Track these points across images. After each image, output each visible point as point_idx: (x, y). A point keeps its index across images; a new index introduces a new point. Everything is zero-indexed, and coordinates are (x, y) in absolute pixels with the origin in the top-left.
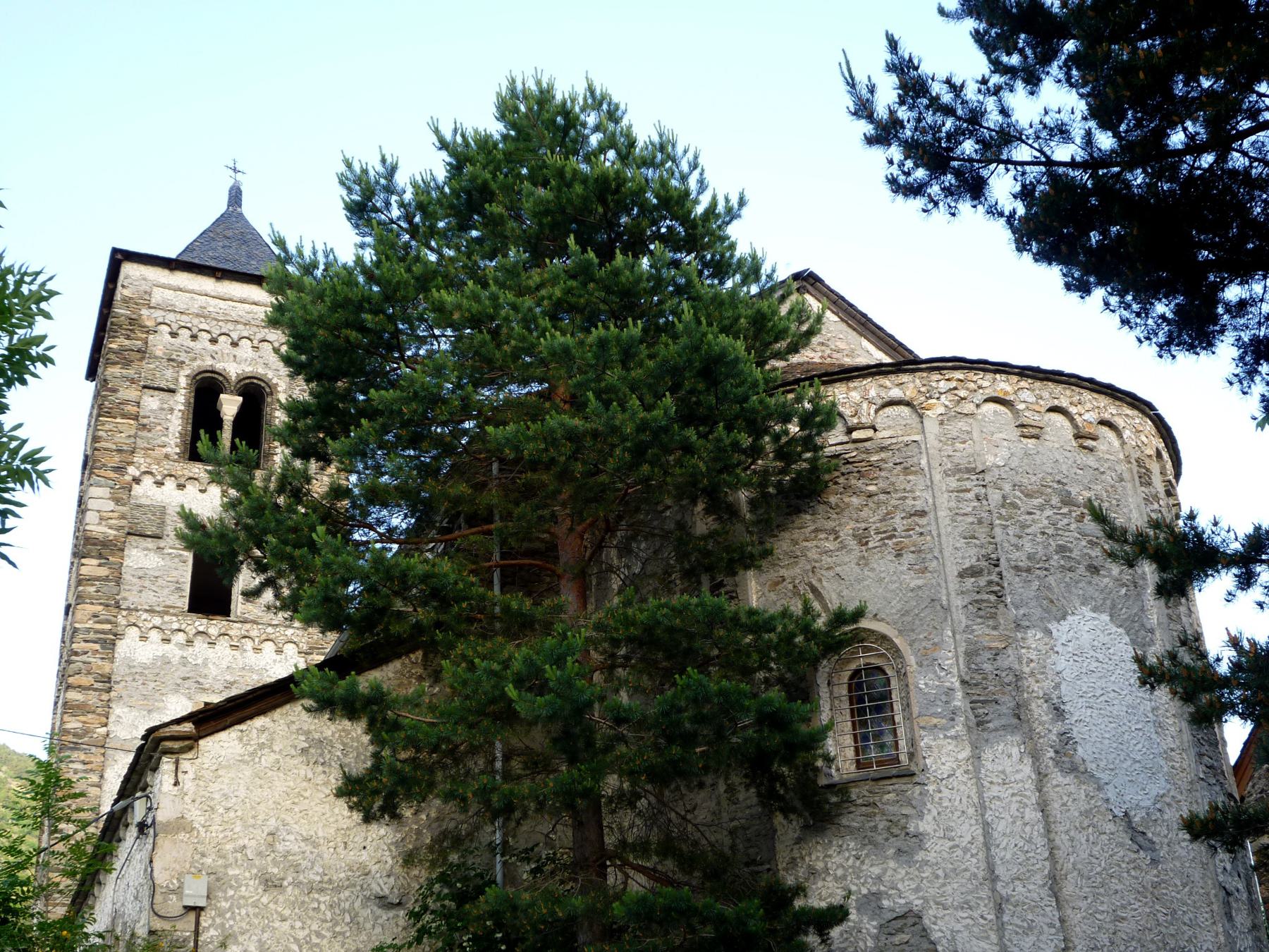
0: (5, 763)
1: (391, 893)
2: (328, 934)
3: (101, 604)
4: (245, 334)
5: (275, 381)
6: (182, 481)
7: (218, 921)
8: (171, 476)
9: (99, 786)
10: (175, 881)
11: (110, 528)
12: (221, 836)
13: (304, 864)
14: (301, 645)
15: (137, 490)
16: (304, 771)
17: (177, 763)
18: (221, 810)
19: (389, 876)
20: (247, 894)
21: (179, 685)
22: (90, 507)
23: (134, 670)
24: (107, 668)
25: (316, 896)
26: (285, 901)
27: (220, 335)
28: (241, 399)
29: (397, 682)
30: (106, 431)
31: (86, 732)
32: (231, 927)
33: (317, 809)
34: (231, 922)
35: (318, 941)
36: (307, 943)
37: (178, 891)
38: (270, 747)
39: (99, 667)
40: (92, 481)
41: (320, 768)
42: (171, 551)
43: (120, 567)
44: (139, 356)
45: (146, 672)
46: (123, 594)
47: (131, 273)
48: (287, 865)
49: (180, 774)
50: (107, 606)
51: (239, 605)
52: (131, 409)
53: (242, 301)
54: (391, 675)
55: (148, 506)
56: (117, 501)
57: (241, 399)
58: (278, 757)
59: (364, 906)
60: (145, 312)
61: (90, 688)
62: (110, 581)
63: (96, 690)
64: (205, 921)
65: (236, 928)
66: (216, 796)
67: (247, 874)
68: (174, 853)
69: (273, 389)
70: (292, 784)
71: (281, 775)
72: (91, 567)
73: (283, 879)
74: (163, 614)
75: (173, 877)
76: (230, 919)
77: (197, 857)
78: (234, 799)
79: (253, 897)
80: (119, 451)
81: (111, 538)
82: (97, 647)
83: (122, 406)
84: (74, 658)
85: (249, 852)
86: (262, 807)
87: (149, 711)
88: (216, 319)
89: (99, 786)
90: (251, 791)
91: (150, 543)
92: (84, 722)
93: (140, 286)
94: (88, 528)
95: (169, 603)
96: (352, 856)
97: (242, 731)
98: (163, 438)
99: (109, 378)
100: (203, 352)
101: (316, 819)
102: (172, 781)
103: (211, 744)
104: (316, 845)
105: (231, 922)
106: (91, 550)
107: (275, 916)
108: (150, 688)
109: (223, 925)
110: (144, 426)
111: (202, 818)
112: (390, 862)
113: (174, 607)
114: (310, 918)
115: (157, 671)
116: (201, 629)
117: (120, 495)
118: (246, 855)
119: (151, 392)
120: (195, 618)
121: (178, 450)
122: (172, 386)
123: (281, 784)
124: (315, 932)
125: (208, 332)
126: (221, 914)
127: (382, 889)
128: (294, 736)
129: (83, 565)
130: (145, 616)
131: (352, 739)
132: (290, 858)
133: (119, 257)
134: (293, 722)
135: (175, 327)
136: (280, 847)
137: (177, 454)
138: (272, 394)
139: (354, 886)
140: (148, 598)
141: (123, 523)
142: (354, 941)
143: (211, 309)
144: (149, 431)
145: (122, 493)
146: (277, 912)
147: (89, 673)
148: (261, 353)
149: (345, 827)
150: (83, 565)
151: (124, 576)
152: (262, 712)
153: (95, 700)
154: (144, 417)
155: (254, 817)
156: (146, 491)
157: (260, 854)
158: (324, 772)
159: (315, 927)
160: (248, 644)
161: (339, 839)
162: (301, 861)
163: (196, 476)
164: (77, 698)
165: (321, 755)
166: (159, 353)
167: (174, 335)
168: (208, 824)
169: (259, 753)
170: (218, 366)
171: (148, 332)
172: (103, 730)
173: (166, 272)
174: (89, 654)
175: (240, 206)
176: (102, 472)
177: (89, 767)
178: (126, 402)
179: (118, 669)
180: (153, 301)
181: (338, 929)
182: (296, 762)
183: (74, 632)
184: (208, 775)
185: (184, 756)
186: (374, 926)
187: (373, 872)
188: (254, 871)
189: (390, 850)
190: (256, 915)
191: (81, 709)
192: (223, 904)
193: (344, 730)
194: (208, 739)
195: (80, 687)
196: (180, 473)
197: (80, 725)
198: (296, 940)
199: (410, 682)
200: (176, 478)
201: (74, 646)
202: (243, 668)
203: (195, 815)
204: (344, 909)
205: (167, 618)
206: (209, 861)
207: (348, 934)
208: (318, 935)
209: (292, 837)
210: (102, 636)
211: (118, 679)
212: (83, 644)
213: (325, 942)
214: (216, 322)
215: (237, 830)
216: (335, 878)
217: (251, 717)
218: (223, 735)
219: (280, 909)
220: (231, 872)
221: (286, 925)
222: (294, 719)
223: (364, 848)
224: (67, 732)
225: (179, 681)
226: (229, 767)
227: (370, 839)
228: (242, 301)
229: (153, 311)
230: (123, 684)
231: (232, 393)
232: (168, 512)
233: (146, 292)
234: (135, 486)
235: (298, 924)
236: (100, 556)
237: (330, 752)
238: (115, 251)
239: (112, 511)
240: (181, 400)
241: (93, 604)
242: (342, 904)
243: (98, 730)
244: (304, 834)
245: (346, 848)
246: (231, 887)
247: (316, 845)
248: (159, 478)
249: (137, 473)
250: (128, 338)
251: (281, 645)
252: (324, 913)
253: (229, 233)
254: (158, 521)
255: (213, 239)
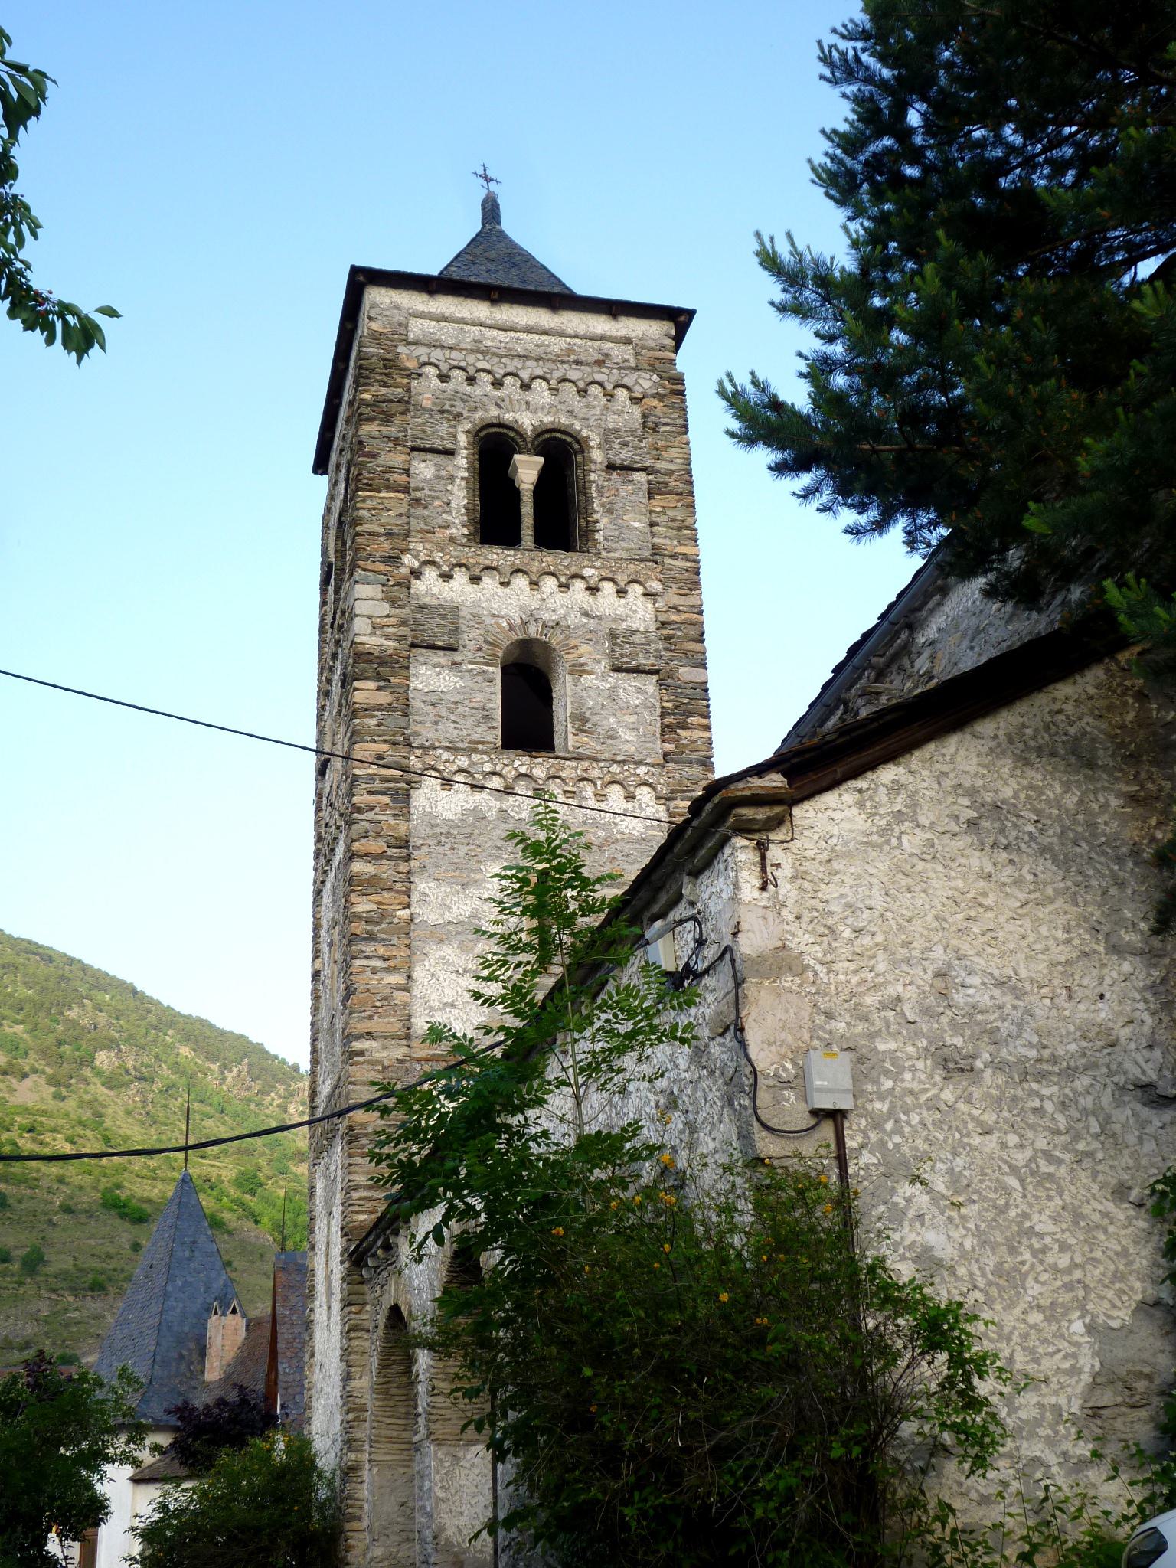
0: (171, 1027)
1: (1161, 1077)
2: (1066, 1157)
3: (385, 741)
4: (539, 372)
5: (585, 433)
6: (477, 571)
7: (873, 1136)
8: (461, 565)
9: (407, 989)
10: (789, 1066)
11: (388, 638)
12: (855, 980)
13: (1005, 1027)
14: (659, 787)
15: (418, 586)
16: (978, 861)
17: (762, 847)
18: (847, 934)
19: (1150, 1047)
20: (915, 1086)
21: (500, 848)
22: (357, 611)
23: (438, 831)
24: (402, 828)
25: (1035, 1086)
26: (983, 1099)
27: (506, 375)
28: (541, 460)
29: (1104, 703)
30: (369, 510)
31: (383, 916)
32: (897, 1146)
33: (1011, 928)
34: (897, 1139)
35: (1051, 1169)
36: (1033, 1173)
37: (800, 1083)
38: (914, 819)
39: (391, 827)
40: (356, 576)
41: (1004, 855)
42: (471, 666)
43: (406, 691)
44: (401, 407)
45: (455, 832)
46: (413, 728)
47: (378, 300)
48: (977, 1030)
49: (769, 869)
50: (394, 744)
51: (570, 736)
52: (398, 478)
53: (529, 330)
54: (1092, 691)
55: (435, 607)
56: (394, 602)
57: (541, 460)
58: (929, 836)
59: (1119, 1104)
60: (402, 349)
61: (382, 856)
62: (394, 710)
63: (390, 858)
64: (852, 1138)
65: (906, 1150)
66: (835, 907)
67: (910, 1049)
68: (780, 1014)
69: (582, 445)
70: (960, 884)
71: (940, 868)
72: (366, 692)
73: (973, 1057)
74: (468, 752)
75: (784, 1057)
76: (893, 1132)
77: (820, 1019)
78: (867, 914)
79: (927, 1090)
80: (389, 535)
81: (390, 652)
82: (386, 799)
83: (386, 476)
84: (356, 816)
85: (907, 1008)
86: (917, 926)
87: (464, 886)
88: (498, 355)
89: (407, 989)
90: (895, 899)
91: (441, 657)
92: (379, 903)
93: (392, 316)
94: (357, 639)
95: (474, 737)
96: (1083, 1011)
97: (860, 791)
98: (445, 516)
99: (364, 439)
100: (485, 399)
101: (1012, 946)
102: (758, 883)
103: (811, 814)
104: (1018, 993)
105: (897, 1139)
106: (364, 670)
107: (970, 1126)
108: (462, 854)
109: (883, 1144)
110: (418, 501)
111: (818, 948)
112: (1149, 1021)
113: (483, 743)
114: (1031, 1127)
115: (469, 830)
116: (523, 770)
117: (396, 594)
118: (903, 1014)
119: (422, 455)
120: (513, 756)
121: (465, 531)
122: (450, 446)
123: (941, 885)
124: (1044, 1152)
125: (489, 372)
126: (877, 1124)
127: (1143, 1072)
128: (950, 799)
129: (356, 689)
130: (446, 755)
131: (1048, 801)
132: (979, 1017)
133: (361, 278)
134: (945, 774)
135: (444, 367)
136: (958, 998)
137: (465, 536)
138: (582, 451)
139: (1095, 1066)
140: (447, 732)
141: (404, 631)
142: (1111, 1167)
143: (489, 343)
144: (425, 507)
145: (398, 591)
146: (973, 1118)
147: (378, 836)
148: (563, 397)
149: (1063, 959)
150: (356, 689)
151: (412, 703)
152: (891, 757)
153: (390, 872)
154: (416, 489)
155: (906, 945)
156: (429, 586)
157: (927, 1011)
158: (1012, 861)
159: (1041, 1144)
160: (588, 790)
161: (1056, 982)
162: (999, 1024)
163: (495, 564)
164: (366, 870)
165: (1002, 831)
166: (427, 404)
167: (444, 378)
168: (829, 958)
169: (897, 829)
170: (506, 416)
171: (409, 376)
172: (404, 913)
173: (424, 297)
174: (377, 810)
175: (499, 223)
176: (369, 565)
177: (391, 963)
178: (392, 469)
179: (417, 828)
180: (411, 336)
181: (1081, 1146)
182: (961, 844)
183: (352, 783)
184: (814, 869)
185: (772, 836)
186: (1140, 1138)
187: (1123, 1040)
188: (923, 1043)
189: (1146, 1001)
190: (938, 1125)
191: (372, 885)
192: (878, 1105)
193: (1032, 787)
194: (806, 805)
195: (368, 856)
196: (472, 561)
197: (374, 907)
198: (1014, 1170)
199: (1125, 704)
200: (468, 569)
201: (355, 799)
202: (584, 822)
203: (803, 941)
204: (1085, 1109)
205: (475, 757)
206: (841, 1026)
207: (1100, 1155)
208: (1050, 1157)
209: (975, 980)
210: (392, 785)
211: (419, 843)
212: (367, 797)
213: (1063, 1171)
214: (497, 359)
215: (881, 967)
216: (1061, 1052)
217: (873, 766)
218: (829, 798)
219: (976, 1113)
220: (882, 1047)
221: (991, 1143)
222: (945, 768)
223: (1102, 996)
224: (357, 917)
225: (500, 843)
226: (847, 855)
227: (1108, 980)
228: (529, 330)
229: (413, 347)
230: (425, 849)
231: (528, 452)
232: (461, 614)
233: (400, 325)
234: (414, 581)
235: (1012, 1139)
236: (378, 677)
237: (1015, 825)
238: (355, 271)
239: (388, 616)
240: (462, 464)
241: (374, 741)
242: (1081, 1100)
243: (399, 913)
244: (996, 973)
245: (1070, 997)
246: (886, 1073)
247: (1018, 993)
248: (446, 568)
249: (416, 564)
250: (384, 385)
251: (632, 789)
252: (1053, 1119)
253: (493, 255)
254: (451, 626)
255: (473, 263)
